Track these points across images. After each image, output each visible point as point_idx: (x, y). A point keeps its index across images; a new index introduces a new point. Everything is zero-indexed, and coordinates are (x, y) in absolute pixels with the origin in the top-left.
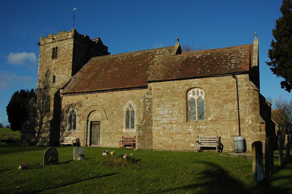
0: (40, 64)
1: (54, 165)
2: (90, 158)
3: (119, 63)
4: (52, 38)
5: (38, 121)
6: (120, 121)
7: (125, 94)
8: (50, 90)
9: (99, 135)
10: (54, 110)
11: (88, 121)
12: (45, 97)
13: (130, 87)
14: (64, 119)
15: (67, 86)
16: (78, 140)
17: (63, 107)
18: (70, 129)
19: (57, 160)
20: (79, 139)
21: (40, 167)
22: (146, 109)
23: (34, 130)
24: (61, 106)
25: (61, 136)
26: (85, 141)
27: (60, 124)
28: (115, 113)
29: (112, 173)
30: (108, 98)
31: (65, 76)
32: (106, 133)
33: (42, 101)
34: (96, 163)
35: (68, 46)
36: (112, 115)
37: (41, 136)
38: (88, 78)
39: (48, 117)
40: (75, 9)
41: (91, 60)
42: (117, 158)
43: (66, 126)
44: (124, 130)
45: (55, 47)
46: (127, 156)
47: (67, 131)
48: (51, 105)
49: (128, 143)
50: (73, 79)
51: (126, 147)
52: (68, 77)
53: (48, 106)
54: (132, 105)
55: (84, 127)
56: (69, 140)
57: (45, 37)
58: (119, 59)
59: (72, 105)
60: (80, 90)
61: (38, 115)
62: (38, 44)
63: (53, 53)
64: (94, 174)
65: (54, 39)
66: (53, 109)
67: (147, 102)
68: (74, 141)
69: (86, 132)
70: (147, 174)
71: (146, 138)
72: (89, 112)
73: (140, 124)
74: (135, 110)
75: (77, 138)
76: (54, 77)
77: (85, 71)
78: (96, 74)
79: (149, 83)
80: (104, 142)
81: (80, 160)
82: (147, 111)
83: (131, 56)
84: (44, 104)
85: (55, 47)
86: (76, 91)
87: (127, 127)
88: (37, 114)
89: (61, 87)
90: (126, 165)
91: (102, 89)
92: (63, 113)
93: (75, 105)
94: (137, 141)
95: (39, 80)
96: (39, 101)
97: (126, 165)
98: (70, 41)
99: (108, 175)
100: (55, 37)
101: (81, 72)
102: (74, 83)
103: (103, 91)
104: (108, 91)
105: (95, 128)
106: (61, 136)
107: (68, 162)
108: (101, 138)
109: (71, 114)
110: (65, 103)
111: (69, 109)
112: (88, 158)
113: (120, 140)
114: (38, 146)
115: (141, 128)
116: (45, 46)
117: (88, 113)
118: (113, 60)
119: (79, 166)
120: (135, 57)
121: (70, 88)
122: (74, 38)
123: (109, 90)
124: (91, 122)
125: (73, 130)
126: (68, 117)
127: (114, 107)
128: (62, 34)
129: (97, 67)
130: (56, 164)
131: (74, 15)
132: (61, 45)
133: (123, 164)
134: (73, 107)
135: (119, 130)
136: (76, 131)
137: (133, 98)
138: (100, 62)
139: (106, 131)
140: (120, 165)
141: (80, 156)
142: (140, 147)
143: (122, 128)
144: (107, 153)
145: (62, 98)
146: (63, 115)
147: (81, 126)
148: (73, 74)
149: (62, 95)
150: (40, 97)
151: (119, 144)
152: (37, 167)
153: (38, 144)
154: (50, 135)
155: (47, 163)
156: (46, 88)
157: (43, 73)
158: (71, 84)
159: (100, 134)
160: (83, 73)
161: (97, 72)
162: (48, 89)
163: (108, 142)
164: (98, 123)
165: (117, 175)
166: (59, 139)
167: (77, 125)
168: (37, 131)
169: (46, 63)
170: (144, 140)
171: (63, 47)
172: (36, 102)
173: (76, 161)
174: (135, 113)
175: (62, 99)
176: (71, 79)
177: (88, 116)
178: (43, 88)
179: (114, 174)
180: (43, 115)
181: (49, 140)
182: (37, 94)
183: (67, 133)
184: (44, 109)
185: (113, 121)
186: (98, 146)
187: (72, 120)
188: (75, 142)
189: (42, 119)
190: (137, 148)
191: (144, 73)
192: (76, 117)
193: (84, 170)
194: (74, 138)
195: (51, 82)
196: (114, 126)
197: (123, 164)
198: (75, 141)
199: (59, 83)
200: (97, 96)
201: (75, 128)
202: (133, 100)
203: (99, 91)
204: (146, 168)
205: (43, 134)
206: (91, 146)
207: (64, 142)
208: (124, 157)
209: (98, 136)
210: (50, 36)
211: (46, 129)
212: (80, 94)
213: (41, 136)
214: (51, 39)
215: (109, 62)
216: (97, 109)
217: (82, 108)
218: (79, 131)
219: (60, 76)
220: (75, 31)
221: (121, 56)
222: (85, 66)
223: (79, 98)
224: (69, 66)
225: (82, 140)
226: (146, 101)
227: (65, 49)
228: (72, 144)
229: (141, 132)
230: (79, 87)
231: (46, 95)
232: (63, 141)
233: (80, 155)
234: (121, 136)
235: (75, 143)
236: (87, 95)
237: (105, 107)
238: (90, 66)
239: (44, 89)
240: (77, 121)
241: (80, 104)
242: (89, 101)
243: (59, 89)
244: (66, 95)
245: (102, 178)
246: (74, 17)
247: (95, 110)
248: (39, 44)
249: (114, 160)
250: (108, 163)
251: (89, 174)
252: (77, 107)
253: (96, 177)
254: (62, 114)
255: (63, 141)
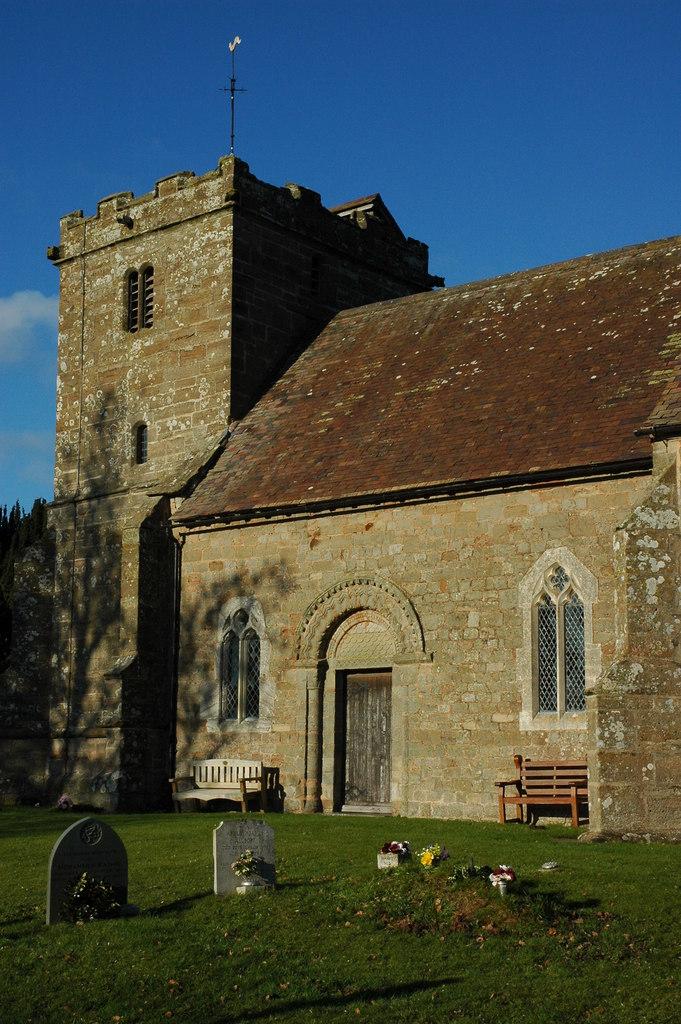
0: (63, 366)
1: (102, 922)
2: (307, 884)
3: (492, 332)
4: (119, 221)
5: (66, 670)
6: (500, 666)
7: (524, 511)
8: (120, 502)
9: (388, 751)
10: (143, 609)
11: (323, 667)
12: (96, 540)
13: (552, 467)
14: (199, 660)
15: (209, 477)
16: (270, 774)
17: (190, 593)
18: (228, 714)
19: (121, 893)
20: (277, 770)
21: (27, 933)
22: (642, 594)
23: (44, 719)
24: (179, 590)
25: (185, 752)
26: (311, 784)
27: (176, 685)
28: (473, 619)
29: (415, 976)
30: (433, 539)
31: (197, 420)
32: (425, 737)
33: (80, 561)
34: (334, 911)
35: (201, 255)
36: (455, 635)
37: (81, 752)
38: (320, 426)
39: (114, 652)
40: (238, 40)
41: (333, 324)
42: (457, 889)
43: (208, 698)
44: (526, 720)
45: (137, 266)
46: (514, 878)
47: (211, 727)
48: (124, 582)
49: (552, 796)
50: (239, 440)
51: (542, 821)
52: (212, 430)
53: (110, 590)
54: (568, 572)
55: (300, 701)
56: (224, 775)
57: (81, 217)
58: (490, 313)
59: (237, 580)
60: (273, 497)
61: (63, 640)
62: (49, 258)
63: (130, 301)
64: (308, 979)
65: (128, 223)
66: (135, 605)
67: (652, 552)
68: (250, 780)
69: (312, 732)
70: (625, 998)
71: (650, 766)
72: (331, 616)
73: (608, 685)
74: (587, 601)
75: (268, 765)
76: (140, 430)
77: (304, 389)
78: (361, 404)
79: (658, 438)
80: (413, 789)
81: (250, 897)
82: (654, 608)
83: (559, 286)
84: (94, 580)
85: (137, 266)
86: (256, 502)
87: (544, 700)
88: (58, 636)
89: (175, 485)
90: (505, 933)
91: (395, 489)
92: (189, 627)
93: (256, 580)
94: (594, 785)
95: (62, 450)
96: (68, 564)
97: (505, 933)
98: (217, 224)
99: (391, 991)
100: (135, 213)
101: (284, 394)
102: (243, 457)
103: (402, 499)
104: (426, 495)
105: (361, 710)
106: (185, 752)
107: (179, 906)
108: (398, 764)
109: (231, 632)
110: (202, 569)
111: (222, 602)
112: (293, 885)
113: (503, 777)
114: (60, 809)
115: (616, 705)
116: (85, 267)
117: (325, 624)
118: (452, 321)
119: (234, 934)
120: (579, 294)
121: (220, 488)
122: (236, 210)
123: (436, 490)
124: (342, 675)
125: (242, 719)
126: (218, 646)
127: (464, 586)
128: (171, 190)
129: (365, 363)
130: (115, 914)
131: (233, 81)
132: (169, 250)
133: (490, 926)
134: (241, 594)
135: (498, 718)
136: (262, 726)
137: (571, 529)
138: (384, 333)
139: (426, 726)
140: (470, 931)
141: (248, 874)
142: (616, 823)
143: (516, 706)
144: (404, 858)
145: (184, 542)
146: (191, 638)
147: (287, 694)
148: (240, 408)
149: (184, 530)
150: (70, 544)
151: (496, 803)
152: (15, 928)
153: (64, 797)
154: (124, 751)
155: (67, 909)
156: (102, 491)
157: (83, 412)
158: (229, 467)
159: (389, 741)
160: (291, 402)
161: (368, 392)
162: (111, 498)
163: (438, 785)
164: (379, 679)
165: (437, 996)
166: (174, 770)
167: (267, 691)
168: (61, 728)
169: (96, 356)
170: (637, 776)
171: (178, 266)
172: (53, 569)
173: (226, 898)
174: (587, 618)
175: (180, 548)
176: (229, 435)
177: (327, 631)
178: (85, 491)
179: (422, 985)
180: (89, 638)
181: (116, 776)
182: (53, 529)
183: (212, 736)
184: (95, 605)
185: (464, 669)
186: (384, 810)
187: (240, 668)
188: (254, 786)
189: (83, 660)
190: (596, 827)
191: (632, 385)
192: (257, 650)
193: (258, 958)
194: (247, 764)
195: (124, 460)
196: (466, 698)
197: (490, 926)
198: (256, 779)
199: (164, 465)
200: (368, 527)
201: (252, 708)
202: (573, 542)
203: (378, 501)
204: (627, 955)
205: (92, 742)
206: (344, 808)
207: (197, 788)
208: (494, 879)
209: (381, 753)
210: (108, 210)
211: (106, 716)
212: (254, 521)
213: (81, 752)
214: (117, 224)
215: (431, 333)
216: (370, 603)
217: (293, 598)
218: (279, 728)
219: (171, 422)
220: (240, 167)
221: (502, 290)
222: (301, 359)
223: (272, 539)
224: (216, 366)
225: (293, 779)
226: (643, 549)
227: (188, 274)
228: (238, 796)
229: (618, 729)
230: (273, 481)
231: (103, 531)
232: (190, 783)
233: (249, 865)
234: (510, 752)
235: (256, 794)
236: (313, 525)
237: (412, 588)
238: (331, 357)
239: (88, 498)
240: (263, 668)
241: (281, 577)
242: (328, 557)
243: (167, 497)
244: (204, 528)
245: (352, 1006)
246: (233, 90)
247: (361, 609)
248: (55, 254)
249: (438, 901)
250: (401, 916)
251: (277, 978)
252: (266, 592)
253: (313, 1003)
254: (183, 633)
255: (193, 779)
